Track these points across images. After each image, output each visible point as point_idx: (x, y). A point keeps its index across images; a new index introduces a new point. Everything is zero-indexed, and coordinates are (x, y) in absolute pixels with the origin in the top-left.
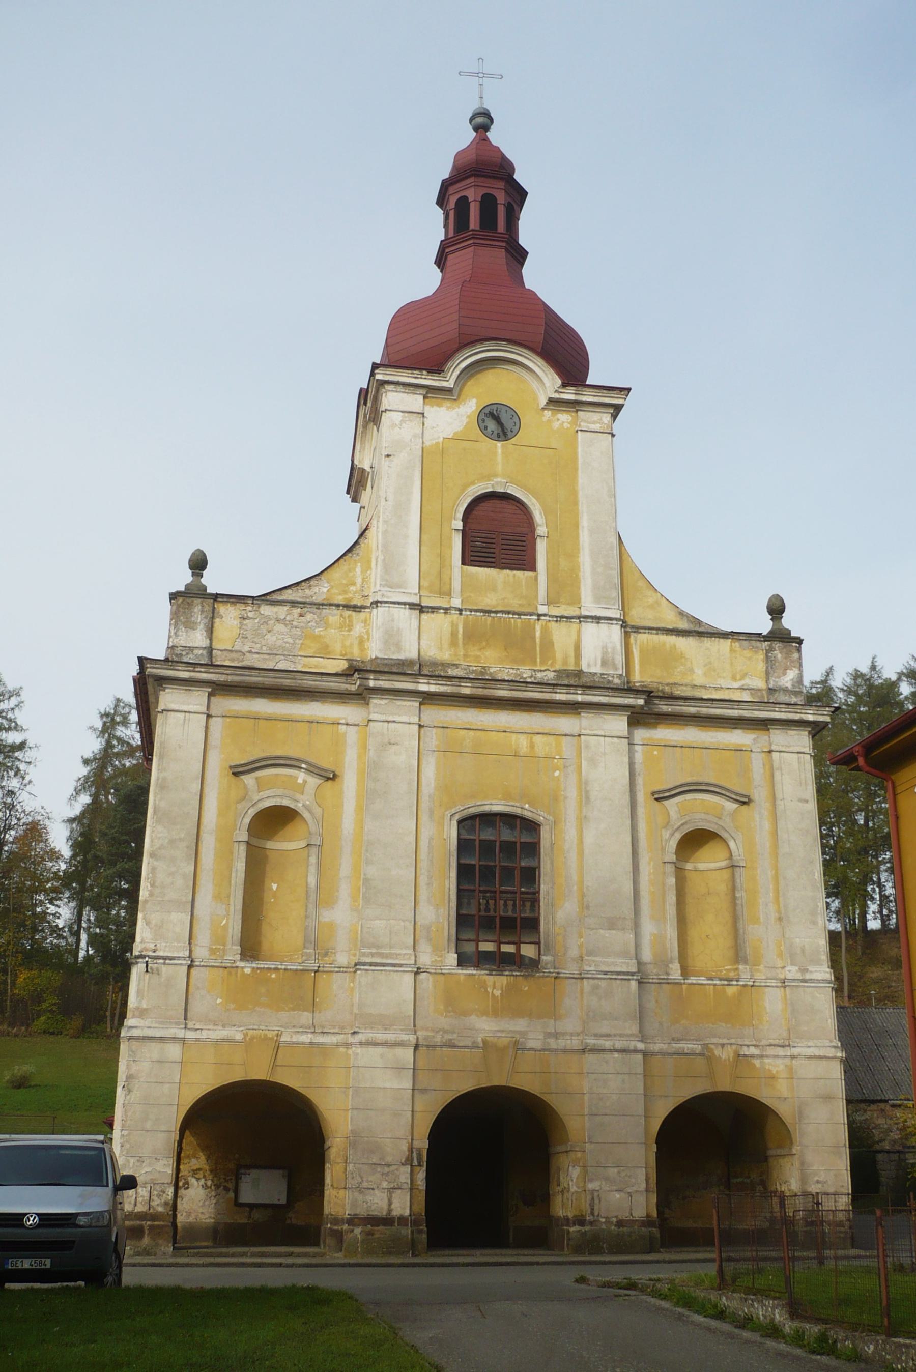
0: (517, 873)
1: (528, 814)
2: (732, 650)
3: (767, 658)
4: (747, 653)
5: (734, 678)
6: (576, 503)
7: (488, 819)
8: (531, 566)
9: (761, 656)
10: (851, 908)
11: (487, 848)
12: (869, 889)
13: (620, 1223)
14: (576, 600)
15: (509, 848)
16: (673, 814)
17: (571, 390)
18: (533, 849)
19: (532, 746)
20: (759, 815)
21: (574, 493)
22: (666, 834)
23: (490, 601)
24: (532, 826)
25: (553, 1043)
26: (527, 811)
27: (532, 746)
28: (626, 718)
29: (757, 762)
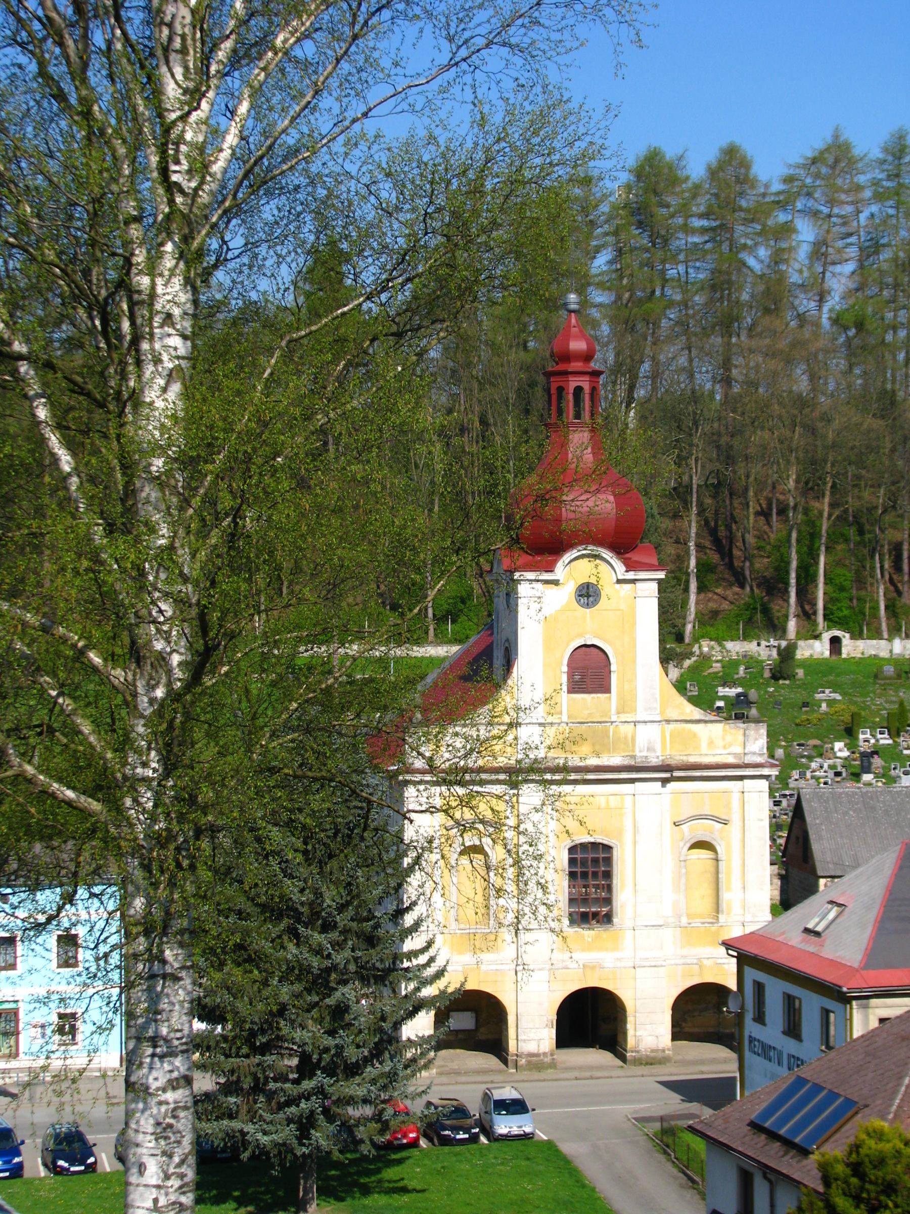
0: (600, 874)
1: (605, 842)
2: (724, 730)
3: (744, 734)
4: (733, 731)
5: (724, 747)
6: (635, 646)
7: (584, 846)
8: (607, 690)
9: (741, 732)
10: (65, 741)
11: (584, 862)
12: (151, 804)
13: (652, 1051)
14: (633, 710)
15: (596, 861)
16: (686, 833)
17: (632, 573)
18: (608, 861)
19: (608, 802)
20: (735, 827)
21: (633, 640)
22: (681, 844)
23: (583, 716)
24: (608, 848)
25: (619, 964)
26: (599, 838)
27: (608, 802)
28: (654, 586)
29: (735, 798)
